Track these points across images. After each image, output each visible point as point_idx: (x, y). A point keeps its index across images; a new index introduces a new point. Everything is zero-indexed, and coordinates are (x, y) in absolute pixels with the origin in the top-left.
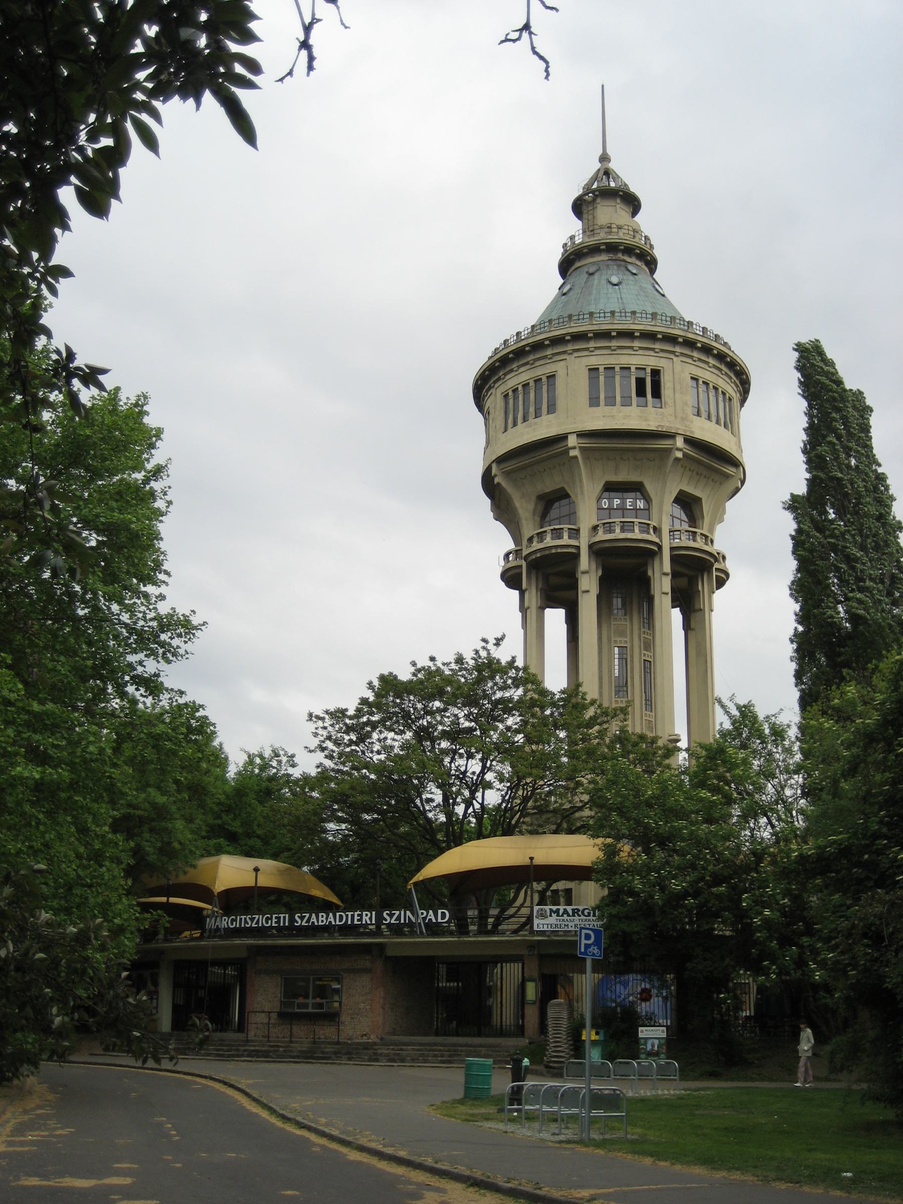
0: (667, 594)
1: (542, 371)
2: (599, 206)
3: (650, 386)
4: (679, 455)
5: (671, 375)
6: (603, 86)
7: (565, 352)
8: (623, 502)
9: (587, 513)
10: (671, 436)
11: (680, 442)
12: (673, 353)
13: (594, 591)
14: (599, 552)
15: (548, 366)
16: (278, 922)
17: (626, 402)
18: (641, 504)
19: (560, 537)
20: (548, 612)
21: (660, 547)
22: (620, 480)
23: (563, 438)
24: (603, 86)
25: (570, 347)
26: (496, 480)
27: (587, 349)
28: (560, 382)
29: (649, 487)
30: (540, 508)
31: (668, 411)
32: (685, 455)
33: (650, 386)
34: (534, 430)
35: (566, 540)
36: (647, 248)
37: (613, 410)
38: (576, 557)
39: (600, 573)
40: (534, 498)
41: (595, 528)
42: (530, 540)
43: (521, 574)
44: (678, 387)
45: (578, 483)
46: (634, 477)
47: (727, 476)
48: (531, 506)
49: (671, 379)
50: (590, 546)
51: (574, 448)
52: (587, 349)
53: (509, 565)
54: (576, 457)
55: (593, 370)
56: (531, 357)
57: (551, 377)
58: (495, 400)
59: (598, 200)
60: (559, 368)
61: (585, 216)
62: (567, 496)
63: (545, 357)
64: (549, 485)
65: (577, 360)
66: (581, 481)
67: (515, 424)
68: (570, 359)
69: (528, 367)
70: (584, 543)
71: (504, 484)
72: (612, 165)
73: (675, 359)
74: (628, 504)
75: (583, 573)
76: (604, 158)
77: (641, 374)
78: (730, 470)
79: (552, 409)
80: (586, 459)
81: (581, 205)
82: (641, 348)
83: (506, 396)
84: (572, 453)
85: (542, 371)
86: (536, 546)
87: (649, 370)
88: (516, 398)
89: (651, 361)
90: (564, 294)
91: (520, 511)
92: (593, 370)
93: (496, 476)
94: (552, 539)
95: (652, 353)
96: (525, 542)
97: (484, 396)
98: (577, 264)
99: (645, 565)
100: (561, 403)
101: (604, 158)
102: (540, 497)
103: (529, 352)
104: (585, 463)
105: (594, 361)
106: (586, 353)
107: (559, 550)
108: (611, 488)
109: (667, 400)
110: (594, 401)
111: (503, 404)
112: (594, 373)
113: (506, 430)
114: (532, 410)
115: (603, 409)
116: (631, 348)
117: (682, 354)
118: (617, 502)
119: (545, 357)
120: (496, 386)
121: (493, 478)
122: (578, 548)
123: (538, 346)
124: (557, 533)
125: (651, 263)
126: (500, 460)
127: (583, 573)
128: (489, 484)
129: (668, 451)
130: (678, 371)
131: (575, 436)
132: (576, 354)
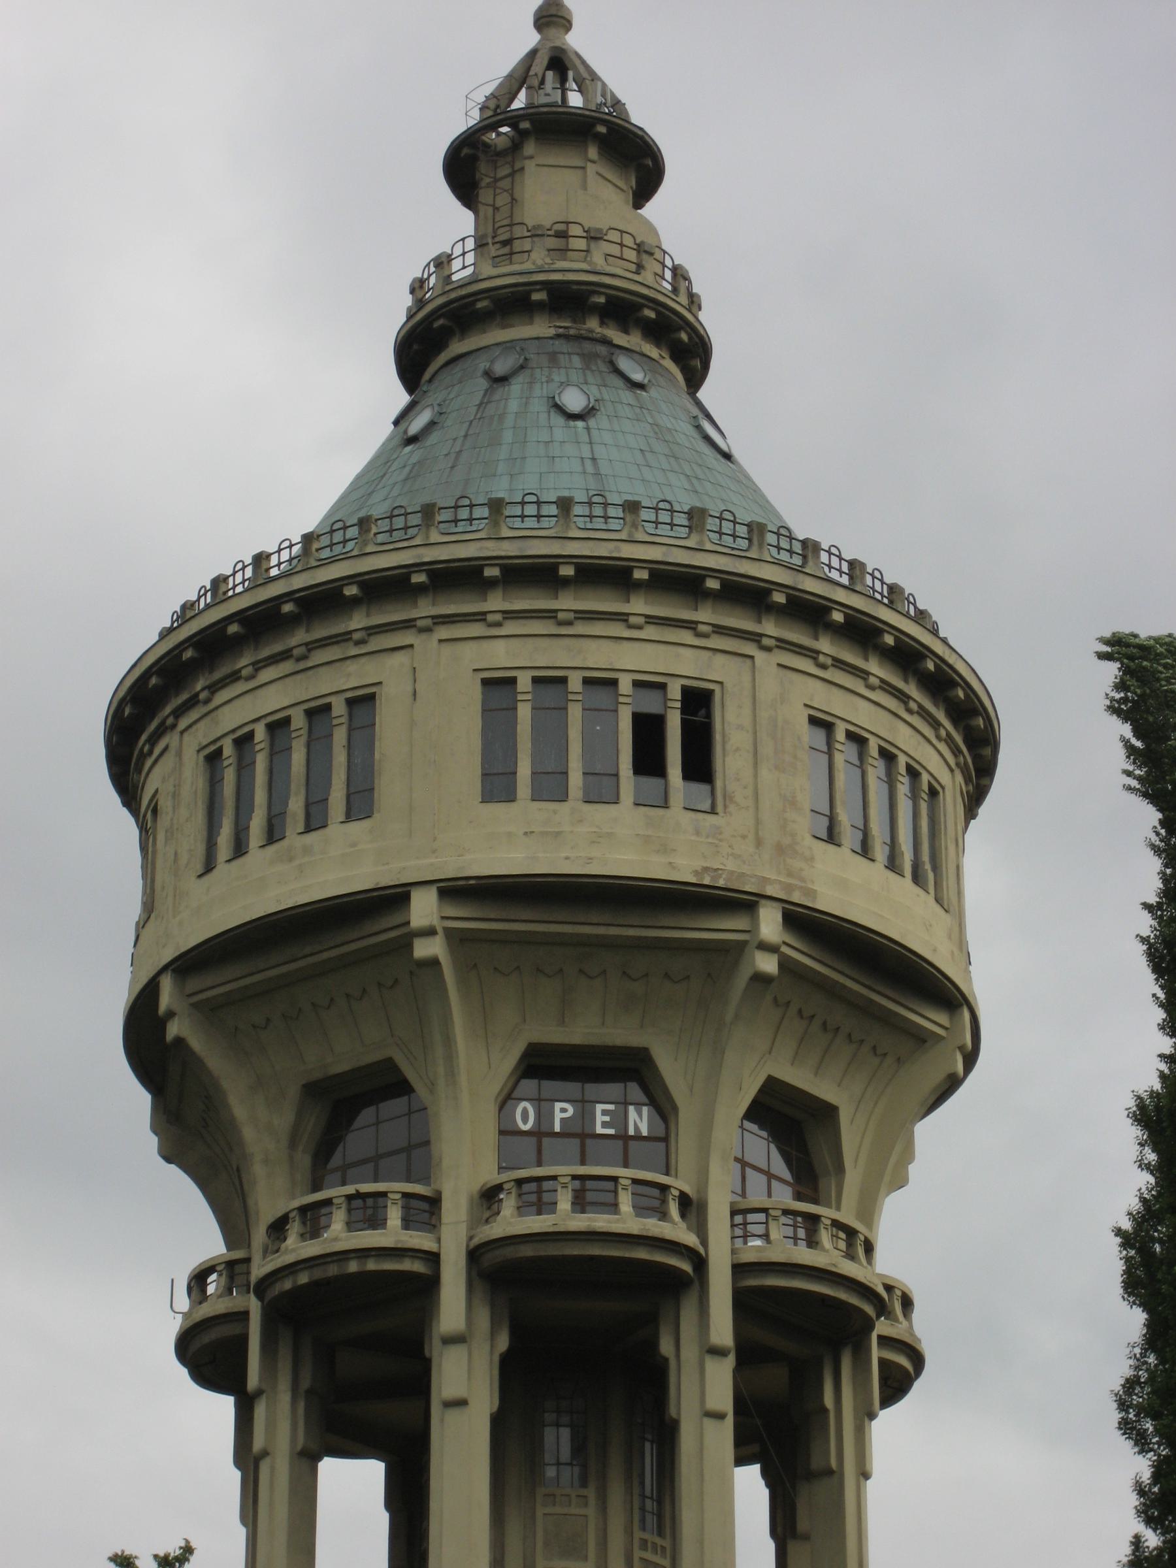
0: (720, 1416)
1: (334, 680)
2: (530, 166)
3: (678, 742)
4: (768, 964)
5: (747, 711)
9: (470, 1129)
10: (743, 903)
11: (770, 924)
12: (755, 638)
15: (352, 667)
19: (376, 1221)
20: (331, 1469)
23: (395, 898)
25: (425, 609)
26: (173, 1030)
28: (389, 718)
29: (670, 1067)
30: (304, 1160)
32: (785, 965)
35: (393, 1232)
36: (679, 305)
38: (424, 1288)
39: (503, 1343)
40: (293, 1091)
41: (490, 1196)
42: (278, 1228)
43: (243, 1340)
44: (767, 748)
46: (620, 1033)
47: (921, 1039)
48: (284, 1120)
49: (747, 721)
50: (474, 1255)
51: (430, 932)
53: (207, 1310)
54: (434, 963)
55: (498, 686)
57: (363, 702)
58: (176, 771)
59: (530, 148)
60: (387, 673)
62: (402, 1087)
64: (344, 1051)
65: (447, 649)
66: (449, 1042)
67: (240, 849)
69: (287, 667)
71: (196, 1043)
72: (575, 40)
73: (760, 657)
74: (600, 1118)
75: (451, 1340)
77: (650, 704)
78: (931, 1019)
79: (361, 804)
80: (467, 968)
81: (474, 159)
82: (651, 620)
83: (213, 758)
84: (423, 949)
85: (334, 680)
86: (296, 1248)
87: (675, 691)
88: (244, 767)
89: (681, 662)
90: (412, 440)
91: (248, 1133)
93: (171, 1014)
94: (350, 1226)
95: (687, 637)
96: (259, 1235)
97: (143, 756)
99: (651, 1320)
102: (315, 1090)
104: (462, 981)
105: (501, 654)
106: (476, 629)
107: (372, 1265)
108: (544, 1065)
109: (732, 786)
110: (497, 785)
111: (201, 784)
113: (209, 866)
115: (525, 811)
117: (784, 645)
118: (562, 1112)
120: (183, 723)
122: (433, 1258)
124: (368, 1210)
125: (691, 354)
126: (186, 965)
127: (451, 1340)
128: (148, 1043)
130: (768, 697)
132: (444, 632)
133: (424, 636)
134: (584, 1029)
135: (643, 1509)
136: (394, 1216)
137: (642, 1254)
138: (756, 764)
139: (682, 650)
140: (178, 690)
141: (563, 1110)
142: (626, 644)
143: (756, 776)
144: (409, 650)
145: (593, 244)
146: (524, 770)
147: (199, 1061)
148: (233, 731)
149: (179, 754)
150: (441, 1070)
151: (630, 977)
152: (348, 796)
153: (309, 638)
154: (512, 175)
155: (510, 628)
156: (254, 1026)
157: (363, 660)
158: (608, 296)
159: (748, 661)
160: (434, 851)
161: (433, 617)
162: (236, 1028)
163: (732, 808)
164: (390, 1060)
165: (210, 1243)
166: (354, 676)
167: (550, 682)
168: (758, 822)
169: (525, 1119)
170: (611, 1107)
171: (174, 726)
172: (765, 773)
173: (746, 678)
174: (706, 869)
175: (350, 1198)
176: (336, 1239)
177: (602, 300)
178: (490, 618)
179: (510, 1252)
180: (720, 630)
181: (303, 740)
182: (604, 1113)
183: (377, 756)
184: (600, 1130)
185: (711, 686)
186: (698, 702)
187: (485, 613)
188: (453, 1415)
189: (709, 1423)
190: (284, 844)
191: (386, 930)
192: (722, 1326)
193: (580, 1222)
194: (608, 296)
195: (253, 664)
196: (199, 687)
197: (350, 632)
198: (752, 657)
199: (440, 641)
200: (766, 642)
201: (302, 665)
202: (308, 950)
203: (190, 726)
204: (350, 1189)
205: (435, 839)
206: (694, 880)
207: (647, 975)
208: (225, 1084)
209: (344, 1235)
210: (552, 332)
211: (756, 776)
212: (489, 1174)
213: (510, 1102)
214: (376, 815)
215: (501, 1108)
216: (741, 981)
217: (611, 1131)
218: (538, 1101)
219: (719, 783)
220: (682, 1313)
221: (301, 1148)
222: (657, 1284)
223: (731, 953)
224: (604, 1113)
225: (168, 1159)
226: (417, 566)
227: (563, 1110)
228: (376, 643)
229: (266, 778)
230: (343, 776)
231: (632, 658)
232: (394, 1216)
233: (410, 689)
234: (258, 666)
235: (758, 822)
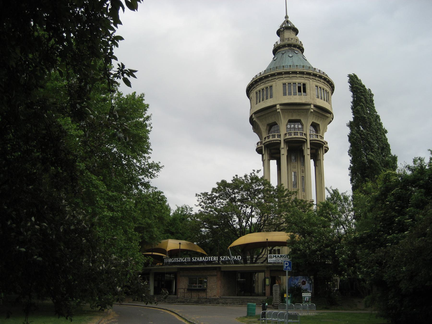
1: (268, 85)
3: (302, 89)
4: (312, 110)
7: (275, 79)
8: (295, 126)
10: (310, 105)
11: (312, 106)
13: (286, 154)
16: (187, 260)
17: (295, 94)
18: (300, 126)
19: (275, 137)
21: (306, 140)
23: (275, 106)
26: (254, 120)
27: (282, 78)
29: (303, 121)
30: (268, 128)
31: (308, 96)
35: (276, 138)
38: (280, 143)
39: (287, 148)
40: (266, 125)
41: (286, 134)
42: (265, 138)
44: (311, 89)
48: (265, 128)
50: (284, 140)
52: (282, 78)
53: (258, 146)
55: (284, 84)
56: (265, 80)
57: (271, 87)
58: (253, 94)
59: (285, 30)
60: (273, 84)
61: (281, 35)
62: (277, 124)
63: (269, 80)
64: (271, 121)
66: (281, 119)
67: (260, 102)
70: (282, 139)
72: (289, 19)
76: (287, 17)
77: (300, 85)
78: (328, 115)
79: (271, 97)
80: (282, 112)
82: (299, 77)
83: (257, 93)
84: (278, 111)
85: (268, 85)
86: (267, 140)
88: (260, 93)
89: (302, 81)
92: (284, 84)
96: (263, 139)
98: (279, 51)
99: (302, 146)
100: (274, 95)
101: (287, 17)
102: (268, 125)
103: (264, 79)
105: (284, 81)
106: (296, 78)
108: (290, 121)
110: (285, 94)
112: (284, 85)
115: (287, 96)
117: (313, 79)
118: (292, 126)
119: (269, 80)
122: (280, 141)
123: (267, 77)
124: (274, 136)
125: (302, 50)
126: (255, 113)
134: (294, 118)
136: (276, 137)
146: (287, 92)
165: (259, 140)
166: (270, 84)
186: (304, 85)
192: (309, 146)
212: (286, 132)
216: (310, 112)
223: (308, 109)
234: (261, 84)
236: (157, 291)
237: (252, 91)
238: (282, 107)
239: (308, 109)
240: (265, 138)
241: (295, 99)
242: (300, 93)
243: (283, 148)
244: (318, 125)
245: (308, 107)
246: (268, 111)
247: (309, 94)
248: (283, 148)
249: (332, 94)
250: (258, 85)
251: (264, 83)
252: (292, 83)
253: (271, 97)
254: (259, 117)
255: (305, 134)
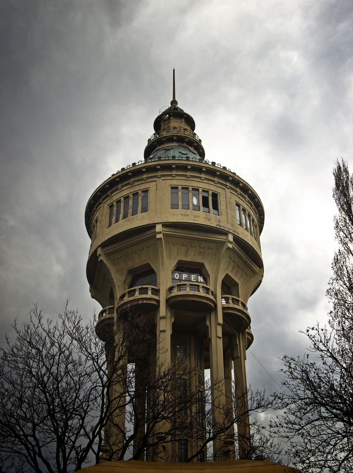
0: (220, 338)
1: (139, 188)
2: (171, 121)
3: (211, 202)
4: (230, 246)
5: (224, 198)
6: (174, 70)
9: (166, 278)
10: (225, 233)
12: (226, 186)
13: (169, 332)
14: (171, 303)
15: (143, 185)
18: (201, 279)
22: (189, 260)
23: (153, 226)
24: (174, 70)
25: (159, 173)
26: (100, 259)
27: (171, 175)
28: (151, 195)
29: (208, 267)
30: (129, 279)
31: (223, 218)
33: (211, 202)
34: (131, 222)
35: (150, 295)
37: (188, 212)
39: (173, 320)
40: (125, 272)
41: (171, 289)
42: (123, 297)
44: (229, 206)
45: (160, 259)
46: (198, 259)
47: (254, 273)
48: (122, 278)
49: (225, 200)
50: (167, 301)
51: (160, 233)
52: (171, 175)
54: (161, 239)
55: (174, 188)
57: (146, 191)
59: (172, 118)
60: (151, 186)
63: (142, 179)
64: (137, 262)
65: (163, 181)
66: (162, 257)
67: (117, 220)
68: (159, 181)
69: (129, 186)
70: (163, 298)
71: (105, 261)
73: (227, 190)
74: (192, 278)
75: (162, 318)
76: (174, 102)
77: (205, 195)
78: (256, 269)
79: (145, 209)
80: (167, 242)
81: (160, 121)
82: (206, 179)
83: (111, 206)
84: (158, 236)
86: (126, 299)
87: (210, 192)
88: (118, 207)
89: (212, 188)
91: (115, 281)
93: (100, 255)
94: (139, 294)
95: (213, 183)
99: (204, 320)
101: (174, 102)
102: (130, 272)
104: (166, 246)
105: (175, 183)
106: (170, 178)
107: (145, 302)
108: (181, 267)
109: (222, 211)
110: (175, 206)
111: (108, 211)
112: (174, 191)
113: (110, 225)
114: (130, 211)
115: (180, 211)
116: (200, 178)
117: (231, 188)
119: (142, 179)
120: (104, 202)
121: (98, 258)
122: (158, 301)
124: (144, 291)
126: (104, 245)
127: (162, 318)
129: (223, 243)
130: (227, 197)
131: (161, 226)
132: (163, 178)
133: (159, 179)
134: (191, 257)
135: (198, 364)
136: (150, 292)
137: (205, 301)
138: (227, 208)
139: (212, 186)
140: (104, 194)
141: (185, 276)
142: (200, 183)
143: (227, 210)
144: (156, 182)
145: (185, 131)
146: (180, 203)
147: (106, 265)
148: (116, 200)
149: (103, 207)
150: (161, 263)
151: (201, 248)
152: (142, 209)
153: (134, 180)
154: (168, 123)
155: (177, 178)
156: (118, 258)
157: (146, 184)
158: (188, 140)
159: (224, 190)
160: (161, 217)
161: (161, 175)
162: (114, 259)
163: (222, 215)
164: (148, 264)
166: (144, 187)
167: (185, 188)
168: (228, 219)
169: (177, 277)
170: (195, 276)
171: (102, 202)
172: (228, 210)
173: (224, 192)
174: (218, 225)
175: (140, 289)
176: (137, 296)
177: (175, 166)
178: (173, 175)
179: (176, 299)
180: (219, 183)
181: (132, 199)
182: (193, 277)
183: (148, 201)
184: (192, 280)
185: (217, 193)
186: (215, 196)
187: (172, 175)
188: (162, 334)
189: (218, 339)
190: (128, 218)
191: (149, 234)
193: (192, 293)
194: (188, 140)
195: (121, 186)
196: (109, 193)
197: (143, 178)
198: (225, 189)
199: (162, 180)
200: (228, 187)
201: (132, 186)
202: (132, 240)
203: (106, 201)
204: (141, 287)
205: (161, 215)
206: (216, 226)
207: (204, 247)
208: (111, 270)
209: (139, 295)
210: (177, 145)
211: (227, 210)
212: (170, 285)
213: (111, 387)
214: (148, 211)
215: (172, 274)
216: (224, 249)
217: (195, 281)
218: (179, 274)
219: (220, 211)
220: (211, 316)
221: (126, 285)
222: (207, 308)
223: (222, 243)
224: (193, 277)
225: (93, 297)
226: (158, 165)
227: (185, 276)
228: (148, 180)
229: (123, 207)
230: (141, 205)
231: (202, 186)
232: (150, 292)
233: (156, 188)
234: (122, 187)
235: (228, 219)
236: (137, 456)
237: (102, 205)
238: (168, 231)
239: (222, 243)
240: (123, 297)
241: (196, 216)
242: (206, 209)
243: (164, 318)
244: (236, 285)
245: (222, 238)
246: (137, 239)
247: (224, 213)
248: (164, 318)
249: (260, 235)
250: (117, 189)
251: (132, 185)
252: (190, 189)
253: (145, 209)
254: (113, 253)
255: (212, 292)
